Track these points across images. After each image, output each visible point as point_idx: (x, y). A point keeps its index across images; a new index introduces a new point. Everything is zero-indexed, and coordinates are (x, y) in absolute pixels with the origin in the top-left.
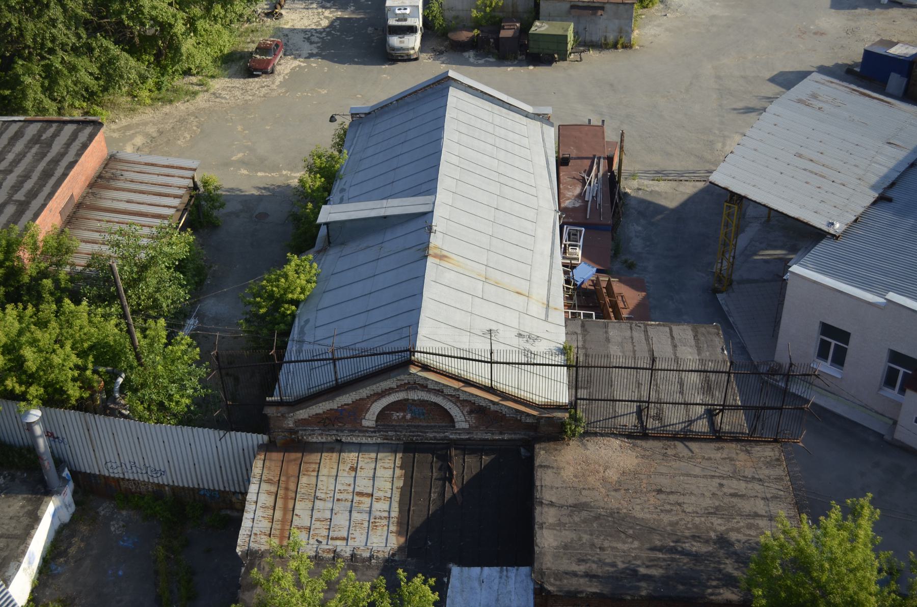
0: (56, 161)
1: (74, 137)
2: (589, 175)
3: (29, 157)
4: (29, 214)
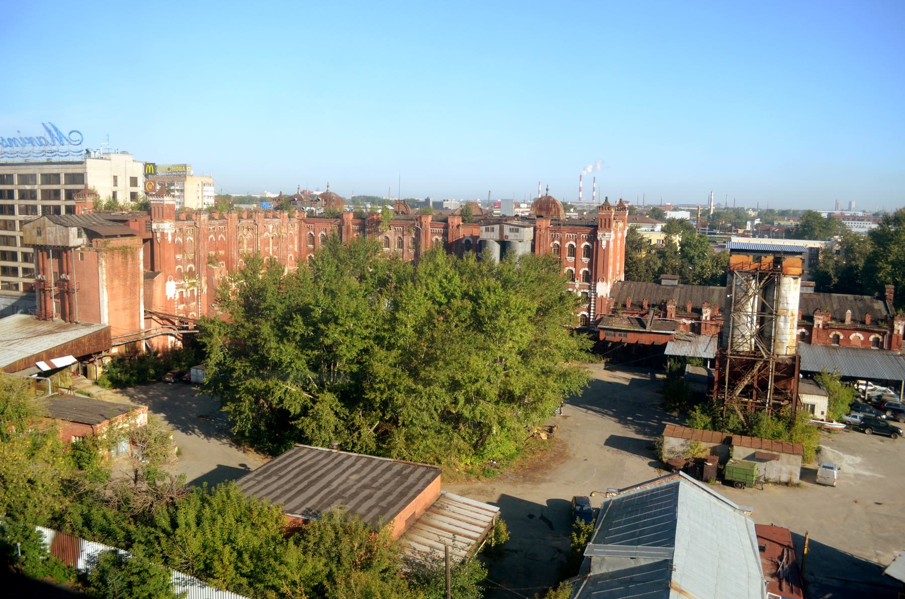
0: (410, 488)
1: (423, 475)
2: (781, 560)
3: (392, 483)
4: (387, 516)
